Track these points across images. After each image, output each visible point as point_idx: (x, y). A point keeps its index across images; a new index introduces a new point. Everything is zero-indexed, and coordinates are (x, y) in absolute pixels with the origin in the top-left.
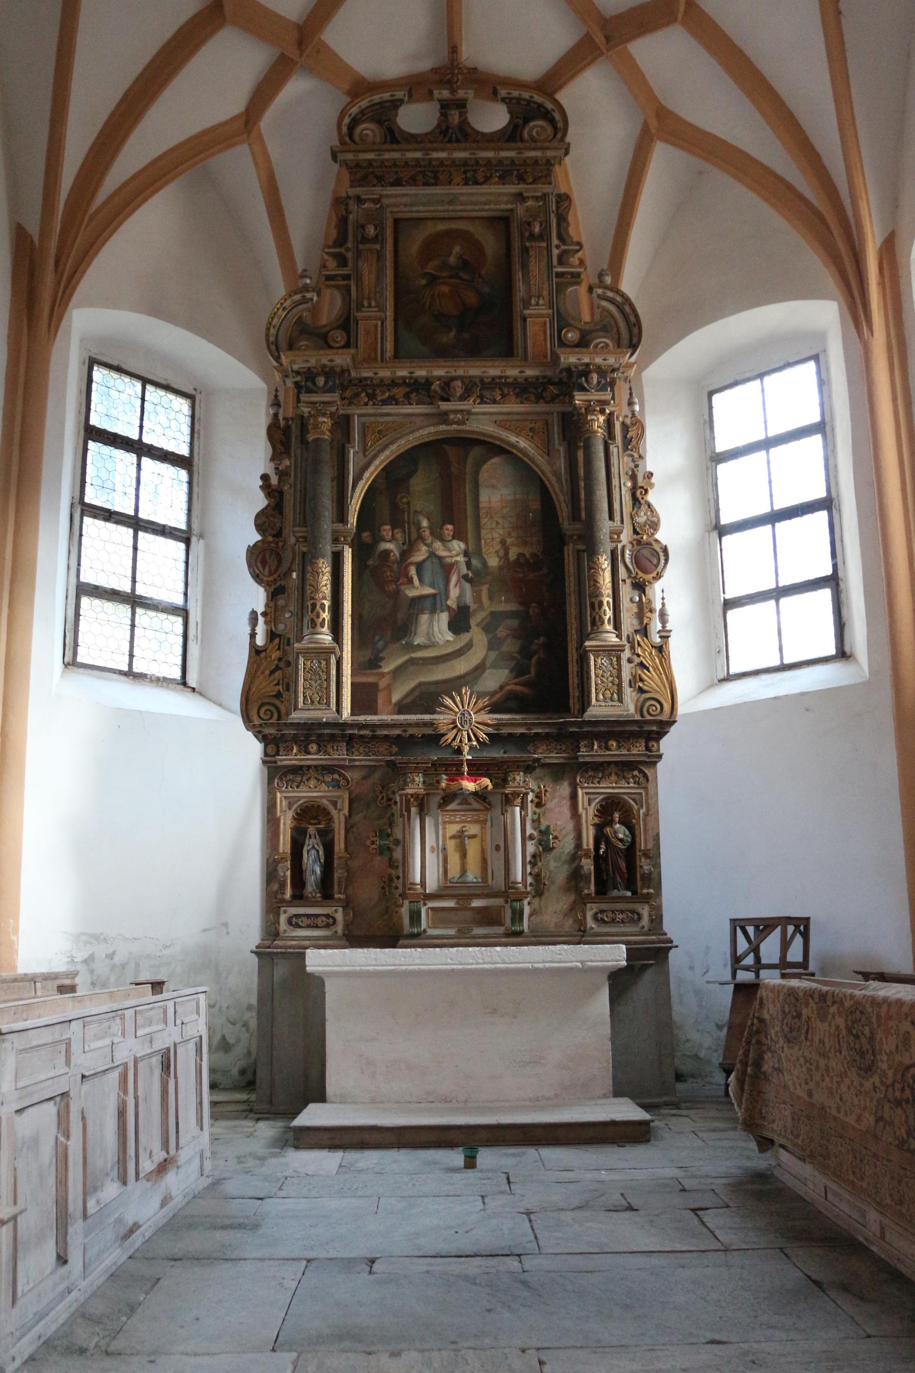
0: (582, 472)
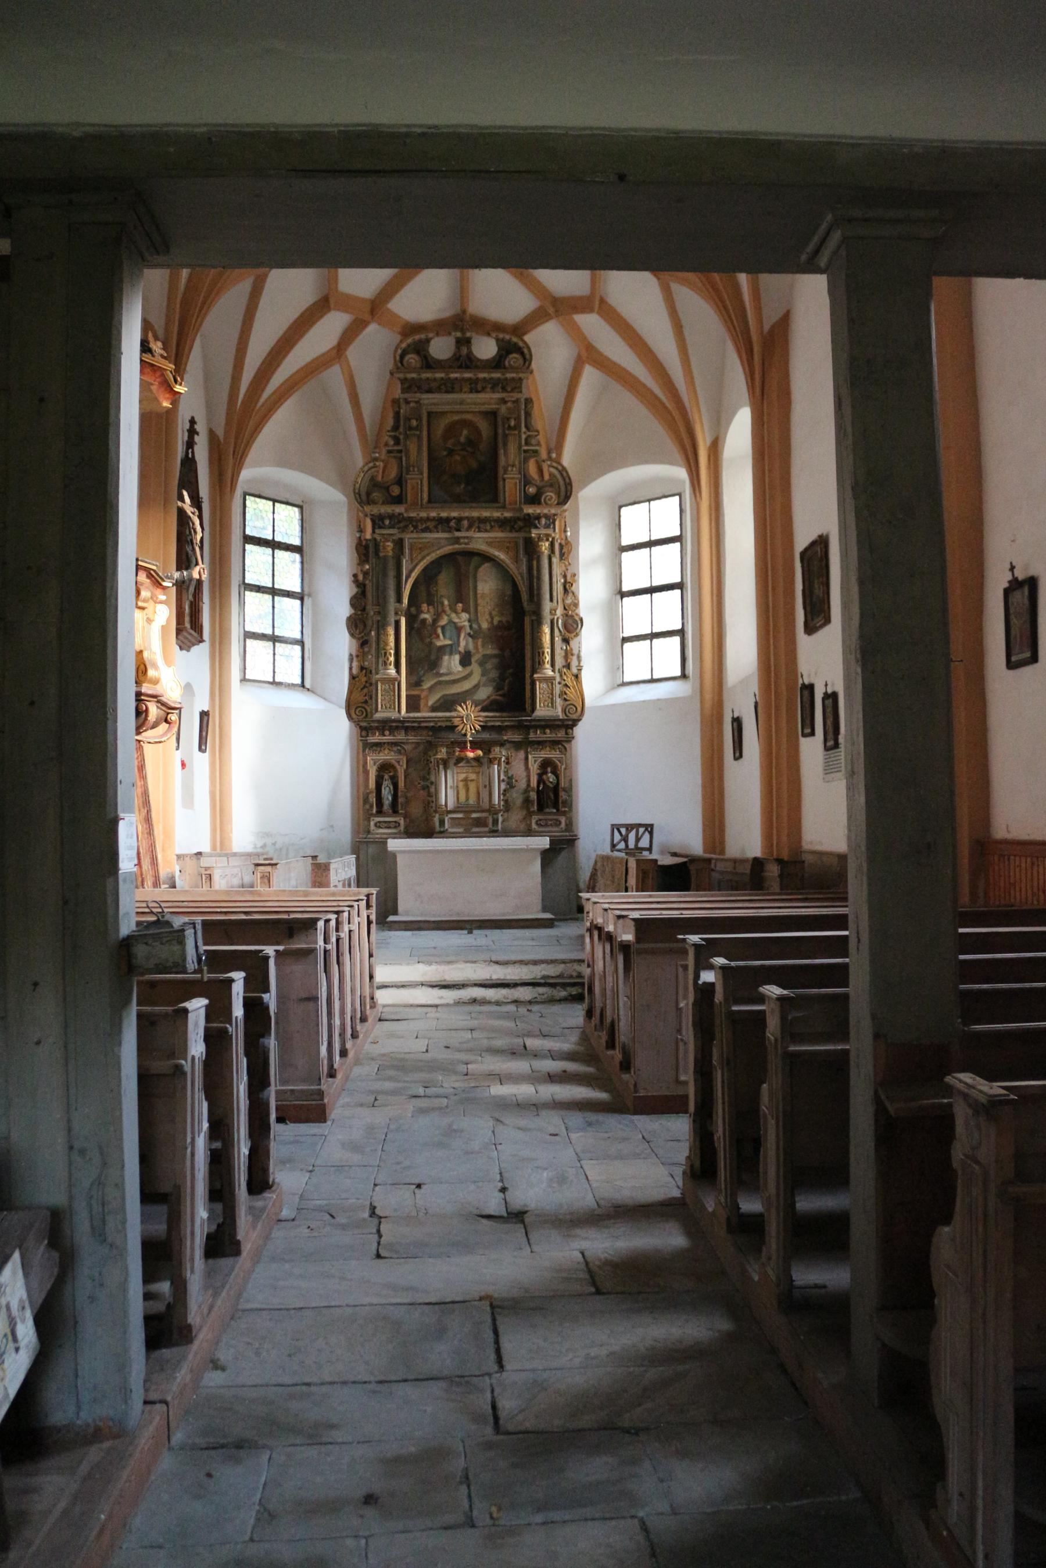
0: (535, 573)
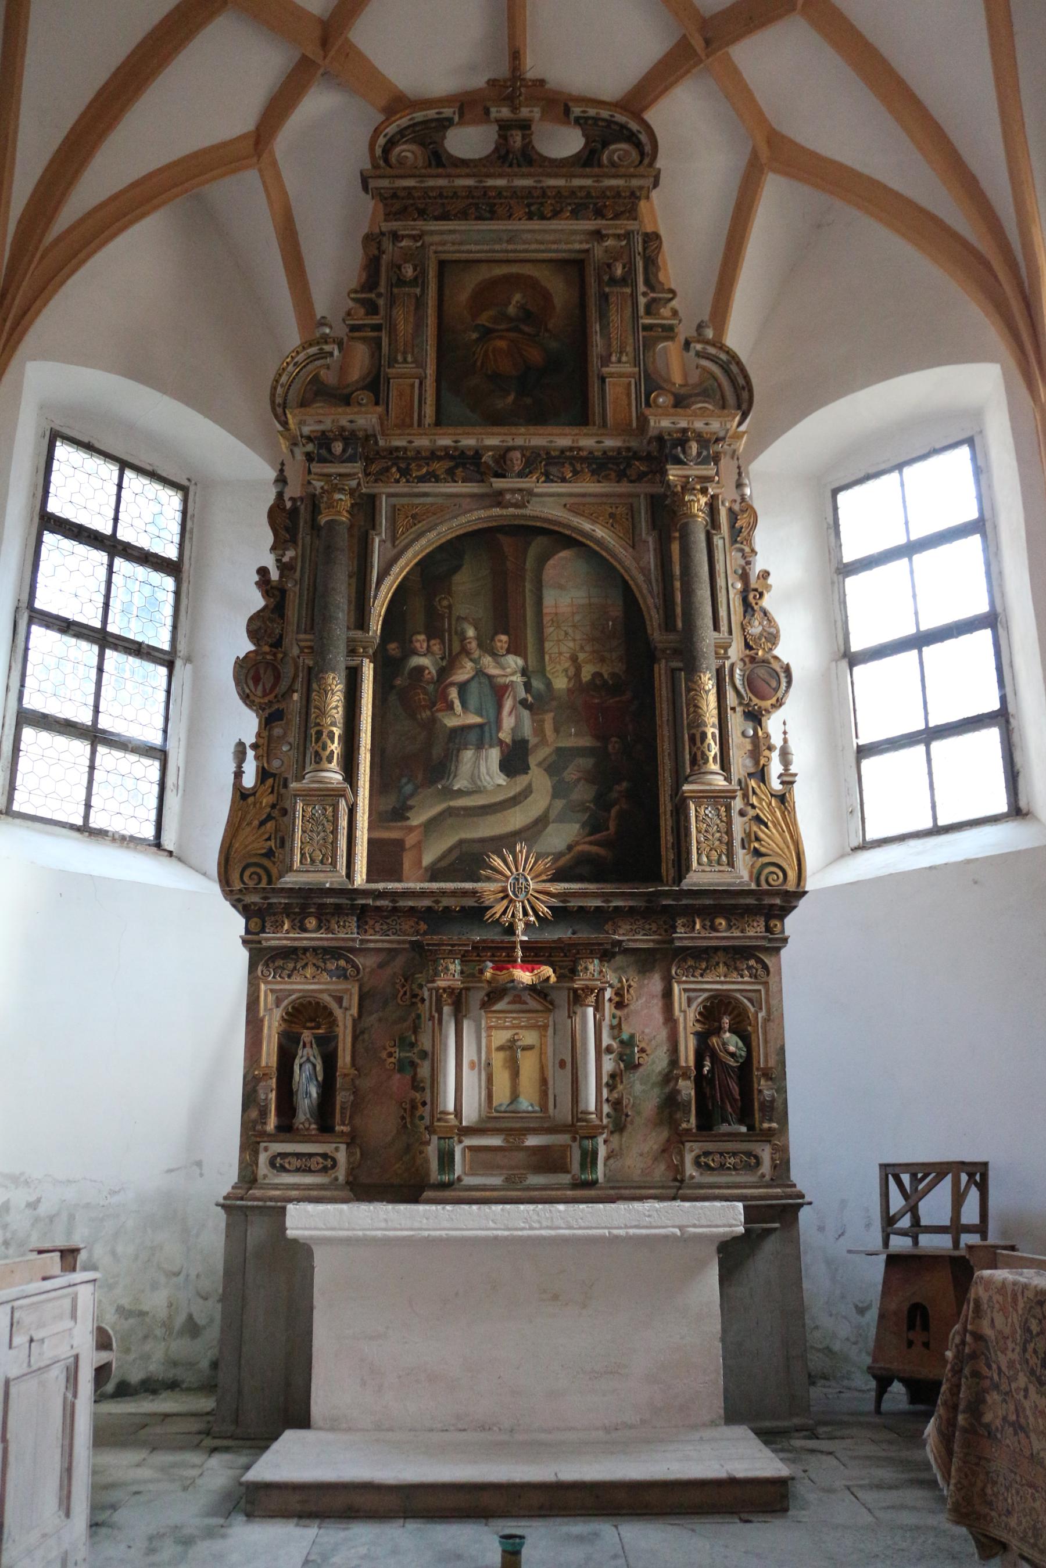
0: (677, 570)
